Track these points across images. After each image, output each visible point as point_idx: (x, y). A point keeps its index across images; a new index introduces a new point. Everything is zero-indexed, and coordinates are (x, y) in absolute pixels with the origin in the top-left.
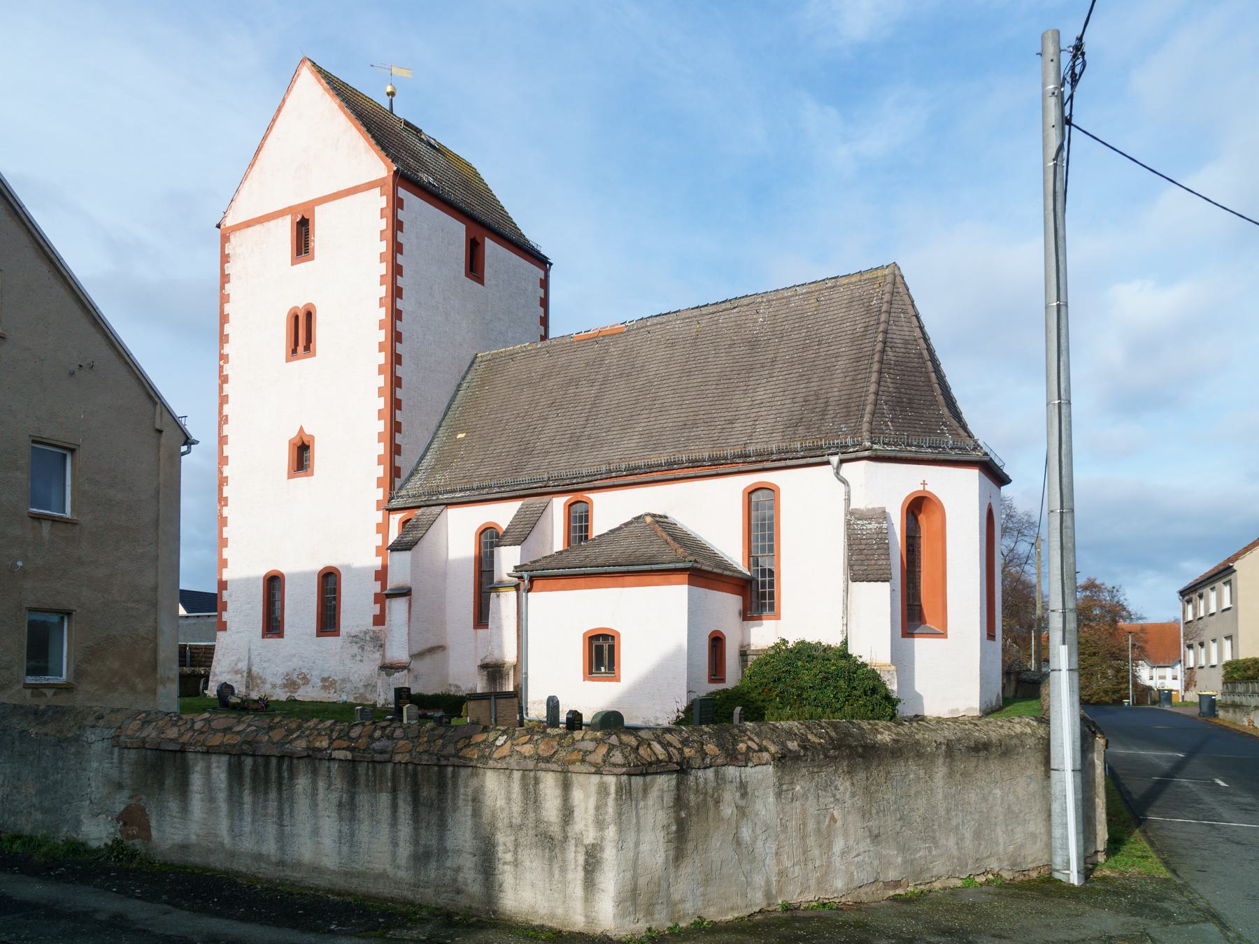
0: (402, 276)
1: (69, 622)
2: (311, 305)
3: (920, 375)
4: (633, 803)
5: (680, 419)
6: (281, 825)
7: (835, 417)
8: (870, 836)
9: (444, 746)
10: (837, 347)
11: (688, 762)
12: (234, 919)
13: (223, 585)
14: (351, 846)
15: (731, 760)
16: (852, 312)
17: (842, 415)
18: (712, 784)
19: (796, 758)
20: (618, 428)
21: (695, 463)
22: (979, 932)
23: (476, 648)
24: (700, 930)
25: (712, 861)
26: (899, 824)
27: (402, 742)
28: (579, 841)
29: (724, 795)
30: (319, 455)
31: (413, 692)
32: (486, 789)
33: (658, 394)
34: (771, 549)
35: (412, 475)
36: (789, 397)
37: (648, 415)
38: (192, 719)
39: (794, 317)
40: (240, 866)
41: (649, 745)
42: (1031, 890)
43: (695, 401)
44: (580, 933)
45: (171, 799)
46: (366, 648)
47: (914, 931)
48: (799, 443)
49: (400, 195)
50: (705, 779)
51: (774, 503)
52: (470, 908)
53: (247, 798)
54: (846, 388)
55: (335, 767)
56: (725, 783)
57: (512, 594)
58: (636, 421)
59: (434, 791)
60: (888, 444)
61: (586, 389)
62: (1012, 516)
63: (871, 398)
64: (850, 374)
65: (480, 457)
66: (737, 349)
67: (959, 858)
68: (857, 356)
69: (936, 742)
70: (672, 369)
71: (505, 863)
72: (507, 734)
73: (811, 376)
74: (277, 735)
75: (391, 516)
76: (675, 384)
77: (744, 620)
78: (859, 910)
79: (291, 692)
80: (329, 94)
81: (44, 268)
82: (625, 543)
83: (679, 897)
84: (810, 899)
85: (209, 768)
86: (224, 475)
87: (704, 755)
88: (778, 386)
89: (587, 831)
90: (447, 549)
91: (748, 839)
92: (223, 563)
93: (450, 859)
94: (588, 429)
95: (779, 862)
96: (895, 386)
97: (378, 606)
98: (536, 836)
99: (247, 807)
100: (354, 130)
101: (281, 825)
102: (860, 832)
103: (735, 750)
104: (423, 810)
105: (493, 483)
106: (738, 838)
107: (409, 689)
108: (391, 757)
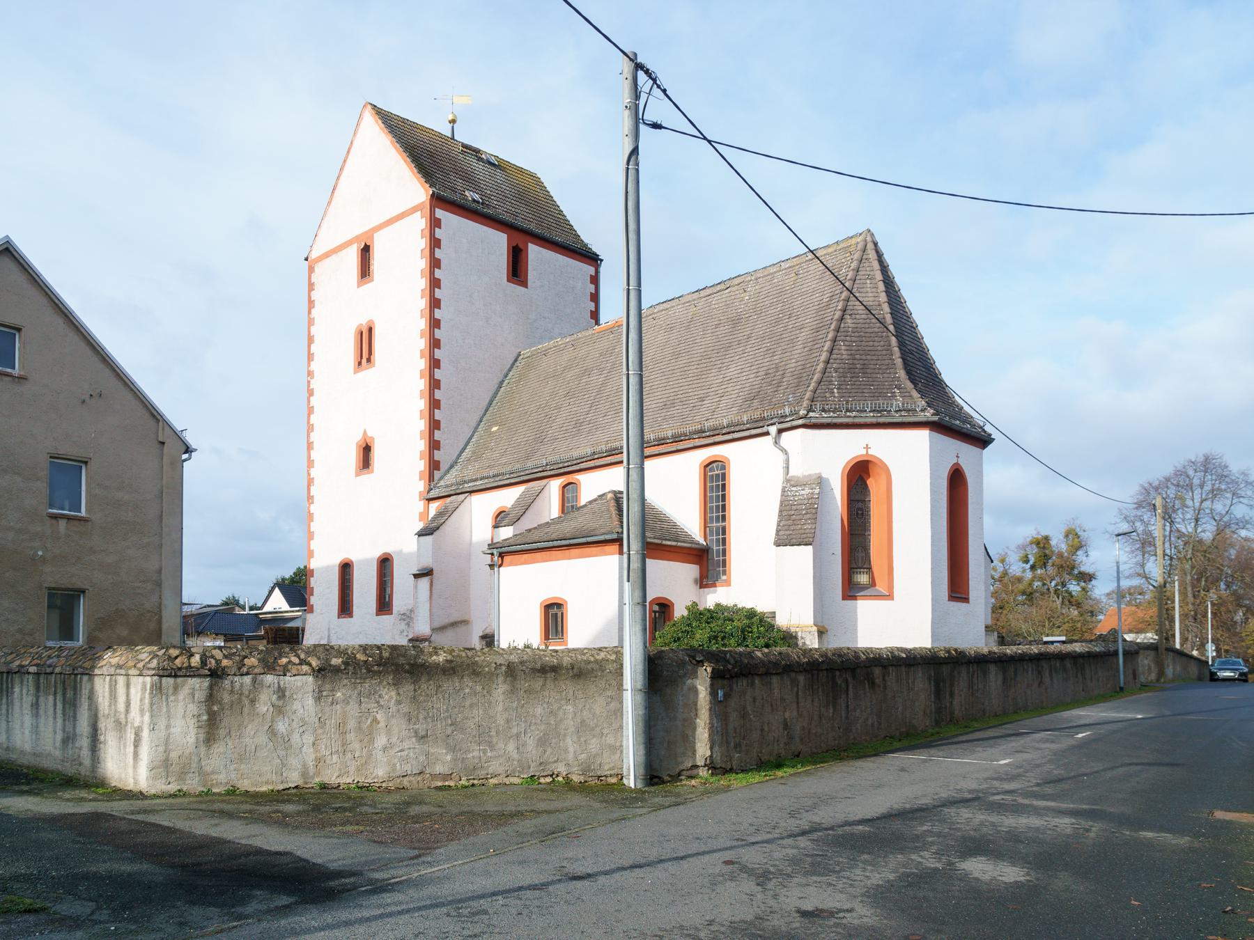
0: (440, 288)
1: (84, 596)
2: (371, 321)
4: (164, 696)
7: (787, 388)
10: (804, 318)
14: (37, 734)
19: (336, 670)
35: (452, 467)
43: (677, 382)
49: (437, 216)
55: (31, 677)
59: (72, 692)
61: (596, 378)
69: (496, 663)
75: (430, 505)
80: (384, 132)
81: (60, 321)
86: (311, 477)
92: (311, 554)
96: (849, 352)
100: (402, 162)
102: (404, 733)
104: (67, 706)
106: (273, 729)
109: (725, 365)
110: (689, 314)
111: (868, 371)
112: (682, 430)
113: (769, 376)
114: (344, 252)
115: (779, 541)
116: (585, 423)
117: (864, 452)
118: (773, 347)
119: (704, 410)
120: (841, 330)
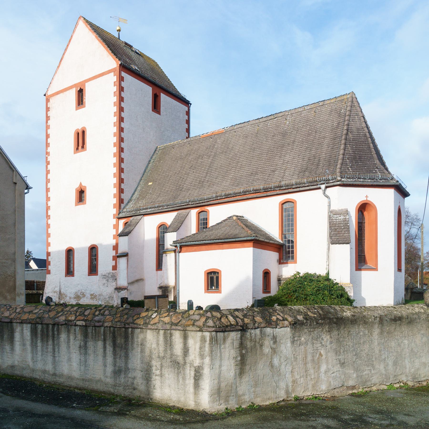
2: (84, 128)
3: (365, 145)
4: (218, 346)
5: (250, 171)
6: (54, 357)
8: (340, 363)
9: (127, 318)
11: (246, 326)
12: (30, 401)
13: (48, 254)
14: (85, 367)
15: (269, 325)
16: (332, 116)
17: (327, 165)
18: (259, 336)
19: (302, 324)
20: (221, 177)
21: (257, 191)
22: (397, 413)
23: (157, 279)
24: (252, 409)
25: (259, 375)
26: (355, 357)
27: (108, 317)
28: (191, 365)
29: (265, 342)
30: (88, 195)
31: (129, 299)
32: (147, 339)
33: (239, 160)
34: (292, 230)
35: (129, 202)
36: (301, 158)
37: (235, 170)
38: (16, 307)
39: (304, 121)
40: (37, 375)
41: (227, 317)
42: (424, 391)
43: (256, 162)
44: (192, 410)
45: (6, 345)
46: (109, 280)
47: (362, 412)
48: (306, 180)
50: (255, 334)
51: (294, 209)
52: (140, 397)
53: (39, 344)
54: (328, 152)
55: (78, 329)
56: (265, 336)
57: (173, 254)
58: (229, 173)
59: (123, 340)
60: (349, 178)
61: (206, 160)
62: (408, 216)
63: (341, 156)
64: (331, 146)
65: (159, 193)
66: (277, 137)
67: (386, 375)
68: (334, 137)
69: (374, 316)
70: (246, 148)
71: (156, 375)
72: (157, 312)
73: (312, 148)
74: (52, 314)
75: (119, 221)
76: (247, 155)
77: (279, 264)
78: (334, 400)
79: (78, 301)
82: (223, 229)
83: (242, 393)
84: (309, 395)
85: (22, 330)
86: (49, 206)
87: (255, 322)
88: (296, 153)
89: (195, 359)
90: (144, 235)
91: (277, 364)
92: (48, 244)
93: (130, 373)
94: (207, 178)
95: (293, 376)
96: (352, 150)
97: (114, 261)
98: (171, 362)
99: (39, 348)
100: (102, 47)
101: (54, 357)
102: (335, 361)
103: (270, 320)
105: (164, 204)
106: (272, 364)
107: (127, 298)
108: (103, 324)
109: (283, 155)
110: (255, 130)
111: (362, 159)
112: (267, 186)
113: (311, 160)
114: (68, 92)
115: (333, 242)
116: (205, 182)
117: (365, 199)
118: (310, 146)
119: (276, 176)
120: (348, 139)
